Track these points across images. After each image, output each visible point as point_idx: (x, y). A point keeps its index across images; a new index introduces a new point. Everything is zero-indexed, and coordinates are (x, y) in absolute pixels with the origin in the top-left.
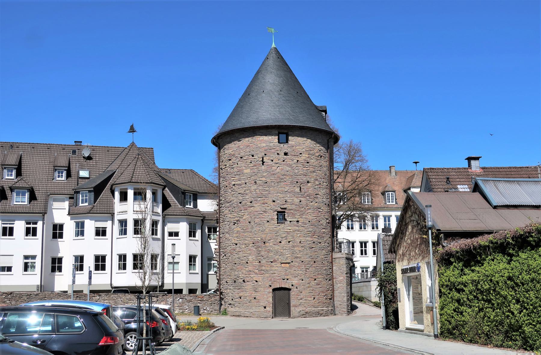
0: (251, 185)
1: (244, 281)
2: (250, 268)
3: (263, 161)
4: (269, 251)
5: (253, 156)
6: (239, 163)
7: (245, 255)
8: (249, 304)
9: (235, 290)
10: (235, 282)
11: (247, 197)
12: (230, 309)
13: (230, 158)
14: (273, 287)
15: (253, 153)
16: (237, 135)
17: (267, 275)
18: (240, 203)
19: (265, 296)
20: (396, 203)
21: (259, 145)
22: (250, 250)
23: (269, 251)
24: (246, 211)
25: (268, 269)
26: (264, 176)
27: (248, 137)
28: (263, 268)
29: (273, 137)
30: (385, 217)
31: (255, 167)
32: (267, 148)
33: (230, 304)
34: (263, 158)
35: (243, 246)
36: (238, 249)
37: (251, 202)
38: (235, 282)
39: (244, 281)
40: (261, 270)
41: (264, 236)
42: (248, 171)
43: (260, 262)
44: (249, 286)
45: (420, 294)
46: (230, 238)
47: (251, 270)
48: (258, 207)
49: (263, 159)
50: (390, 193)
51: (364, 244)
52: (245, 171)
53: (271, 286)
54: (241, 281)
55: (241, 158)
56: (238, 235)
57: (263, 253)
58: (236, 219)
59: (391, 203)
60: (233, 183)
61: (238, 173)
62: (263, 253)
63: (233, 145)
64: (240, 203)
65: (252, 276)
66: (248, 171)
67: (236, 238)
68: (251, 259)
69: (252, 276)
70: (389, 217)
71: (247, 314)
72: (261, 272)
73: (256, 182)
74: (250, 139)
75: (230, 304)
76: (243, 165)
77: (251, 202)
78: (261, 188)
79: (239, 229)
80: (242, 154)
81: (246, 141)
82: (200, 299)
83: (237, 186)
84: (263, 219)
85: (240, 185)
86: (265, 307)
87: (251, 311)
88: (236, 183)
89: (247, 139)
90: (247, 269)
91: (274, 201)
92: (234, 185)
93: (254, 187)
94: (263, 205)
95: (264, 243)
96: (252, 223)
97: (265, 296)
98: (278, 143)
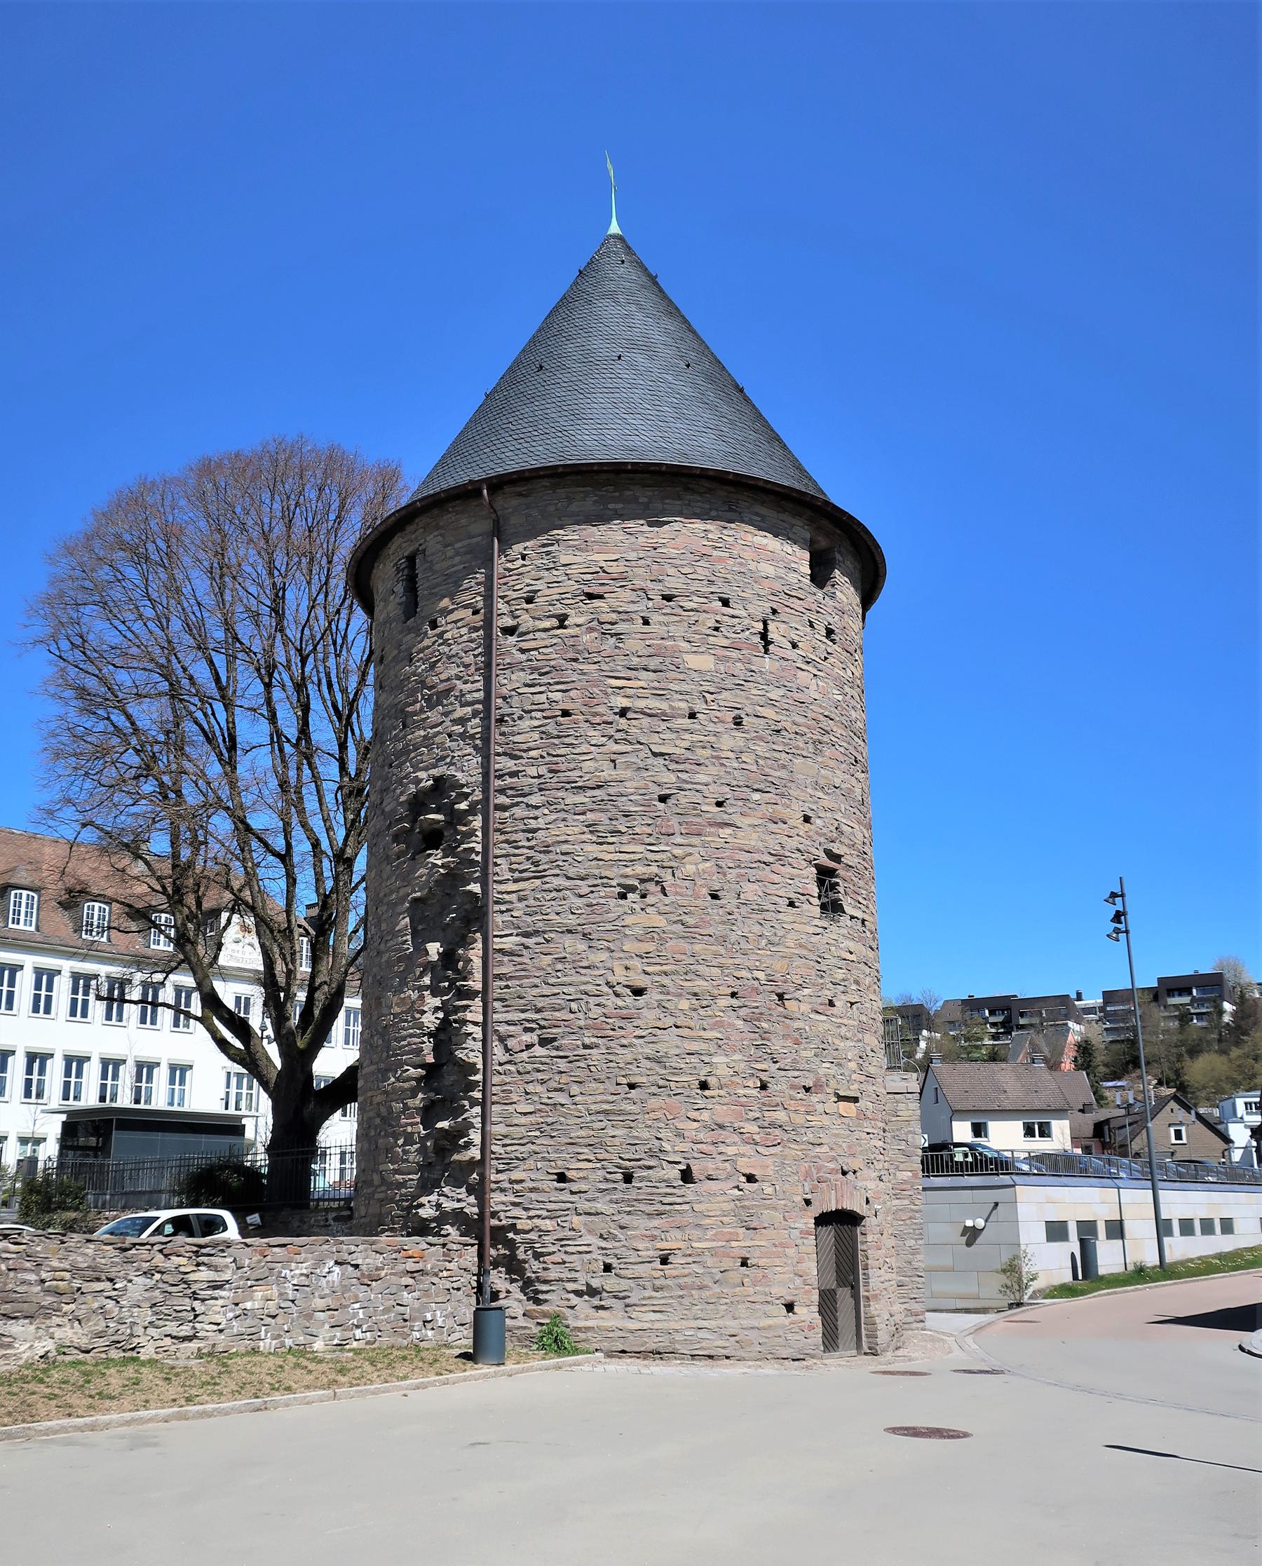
0: (720, 728)
1: (687, 1176)
2: (723, 1113)
3: (764, 635)
4: (799, 1039)
5: (726, 603)
6: (654, 618)
7: (694, 1047)
8: (717, 1289)
9: (625, 1220)
10: (628, 1178)
11: (702, 778)
12: (583, 1315)
13: (596, 590)
14: (816, 1210)
15: (728, 592)
16: (643, 495)
17: (794, 1151)
18: (663, 799)
19: (791, 1252)
20: (38, 929)
21: (752, 566)
22: (718, 1025)
23: (799, 1039)
24: (695, 840)
25: (799, 1119)
26: (772, 703)
27: (704, 516)
28: (781, 1116)
29: (796, 548)
30: (39, 972)
31: (735, 654)
32: (777, 586)
33: (592, 1292)
34: (765, 623)
35: (684, 1004)
36: (649, 1016)
37: (719, 804)
38: (628, 1178)
39: (687, 1176)
40: (773, 1125)
41: (779, 965)
42: (704, 662)
43: (764, 1087)
44: (714, 1199)
45: (1220, 1256)
46: (596, 957)
47: (725, 1120)
48: (750, 834)
49: (765, 628)
50: (25, 893)
51: (36, 1060)
52: (693, 661)
53: (808, 1202)
54: (674, 1173)
55: (668, 598)
56: (650, 947)
57: (776, 1045)
58: (640, 869)
59: (21, 926)
60: (622, 702)
61: (653, 663)
62: (776, 1045)
63: (620, 536)
64: (663, 799)
65: (731, 1150)
66: (704, 662)
67: (636, 963)
68: (723, 1071)
69: (731, 1150)
70: (53, 974)
71: (714, 1343)
72: (773, 1133)
73: (738, 722)
74: (711, 526)
75: (592, 1292)
76: (677, 630)
77: (719, 804)
78: (761, 748)
79: (660, 922)
80: (674, 583)
81: (687, 535)
82: (411, 1266)
83: (646, 721)
84: (772, 889)
85: (664, 717)
86: (790, 1307)
87: (732, 1325)
88: (641, 704)
89: (698, 525)
90: (705, 1116)
91: (807, 819)
92: (623, 712)
93: (730, 740)
94: (772, 827)
95: (781, 996)
96: (728, 900)
97: (791, 1252)
98: (807, 581)
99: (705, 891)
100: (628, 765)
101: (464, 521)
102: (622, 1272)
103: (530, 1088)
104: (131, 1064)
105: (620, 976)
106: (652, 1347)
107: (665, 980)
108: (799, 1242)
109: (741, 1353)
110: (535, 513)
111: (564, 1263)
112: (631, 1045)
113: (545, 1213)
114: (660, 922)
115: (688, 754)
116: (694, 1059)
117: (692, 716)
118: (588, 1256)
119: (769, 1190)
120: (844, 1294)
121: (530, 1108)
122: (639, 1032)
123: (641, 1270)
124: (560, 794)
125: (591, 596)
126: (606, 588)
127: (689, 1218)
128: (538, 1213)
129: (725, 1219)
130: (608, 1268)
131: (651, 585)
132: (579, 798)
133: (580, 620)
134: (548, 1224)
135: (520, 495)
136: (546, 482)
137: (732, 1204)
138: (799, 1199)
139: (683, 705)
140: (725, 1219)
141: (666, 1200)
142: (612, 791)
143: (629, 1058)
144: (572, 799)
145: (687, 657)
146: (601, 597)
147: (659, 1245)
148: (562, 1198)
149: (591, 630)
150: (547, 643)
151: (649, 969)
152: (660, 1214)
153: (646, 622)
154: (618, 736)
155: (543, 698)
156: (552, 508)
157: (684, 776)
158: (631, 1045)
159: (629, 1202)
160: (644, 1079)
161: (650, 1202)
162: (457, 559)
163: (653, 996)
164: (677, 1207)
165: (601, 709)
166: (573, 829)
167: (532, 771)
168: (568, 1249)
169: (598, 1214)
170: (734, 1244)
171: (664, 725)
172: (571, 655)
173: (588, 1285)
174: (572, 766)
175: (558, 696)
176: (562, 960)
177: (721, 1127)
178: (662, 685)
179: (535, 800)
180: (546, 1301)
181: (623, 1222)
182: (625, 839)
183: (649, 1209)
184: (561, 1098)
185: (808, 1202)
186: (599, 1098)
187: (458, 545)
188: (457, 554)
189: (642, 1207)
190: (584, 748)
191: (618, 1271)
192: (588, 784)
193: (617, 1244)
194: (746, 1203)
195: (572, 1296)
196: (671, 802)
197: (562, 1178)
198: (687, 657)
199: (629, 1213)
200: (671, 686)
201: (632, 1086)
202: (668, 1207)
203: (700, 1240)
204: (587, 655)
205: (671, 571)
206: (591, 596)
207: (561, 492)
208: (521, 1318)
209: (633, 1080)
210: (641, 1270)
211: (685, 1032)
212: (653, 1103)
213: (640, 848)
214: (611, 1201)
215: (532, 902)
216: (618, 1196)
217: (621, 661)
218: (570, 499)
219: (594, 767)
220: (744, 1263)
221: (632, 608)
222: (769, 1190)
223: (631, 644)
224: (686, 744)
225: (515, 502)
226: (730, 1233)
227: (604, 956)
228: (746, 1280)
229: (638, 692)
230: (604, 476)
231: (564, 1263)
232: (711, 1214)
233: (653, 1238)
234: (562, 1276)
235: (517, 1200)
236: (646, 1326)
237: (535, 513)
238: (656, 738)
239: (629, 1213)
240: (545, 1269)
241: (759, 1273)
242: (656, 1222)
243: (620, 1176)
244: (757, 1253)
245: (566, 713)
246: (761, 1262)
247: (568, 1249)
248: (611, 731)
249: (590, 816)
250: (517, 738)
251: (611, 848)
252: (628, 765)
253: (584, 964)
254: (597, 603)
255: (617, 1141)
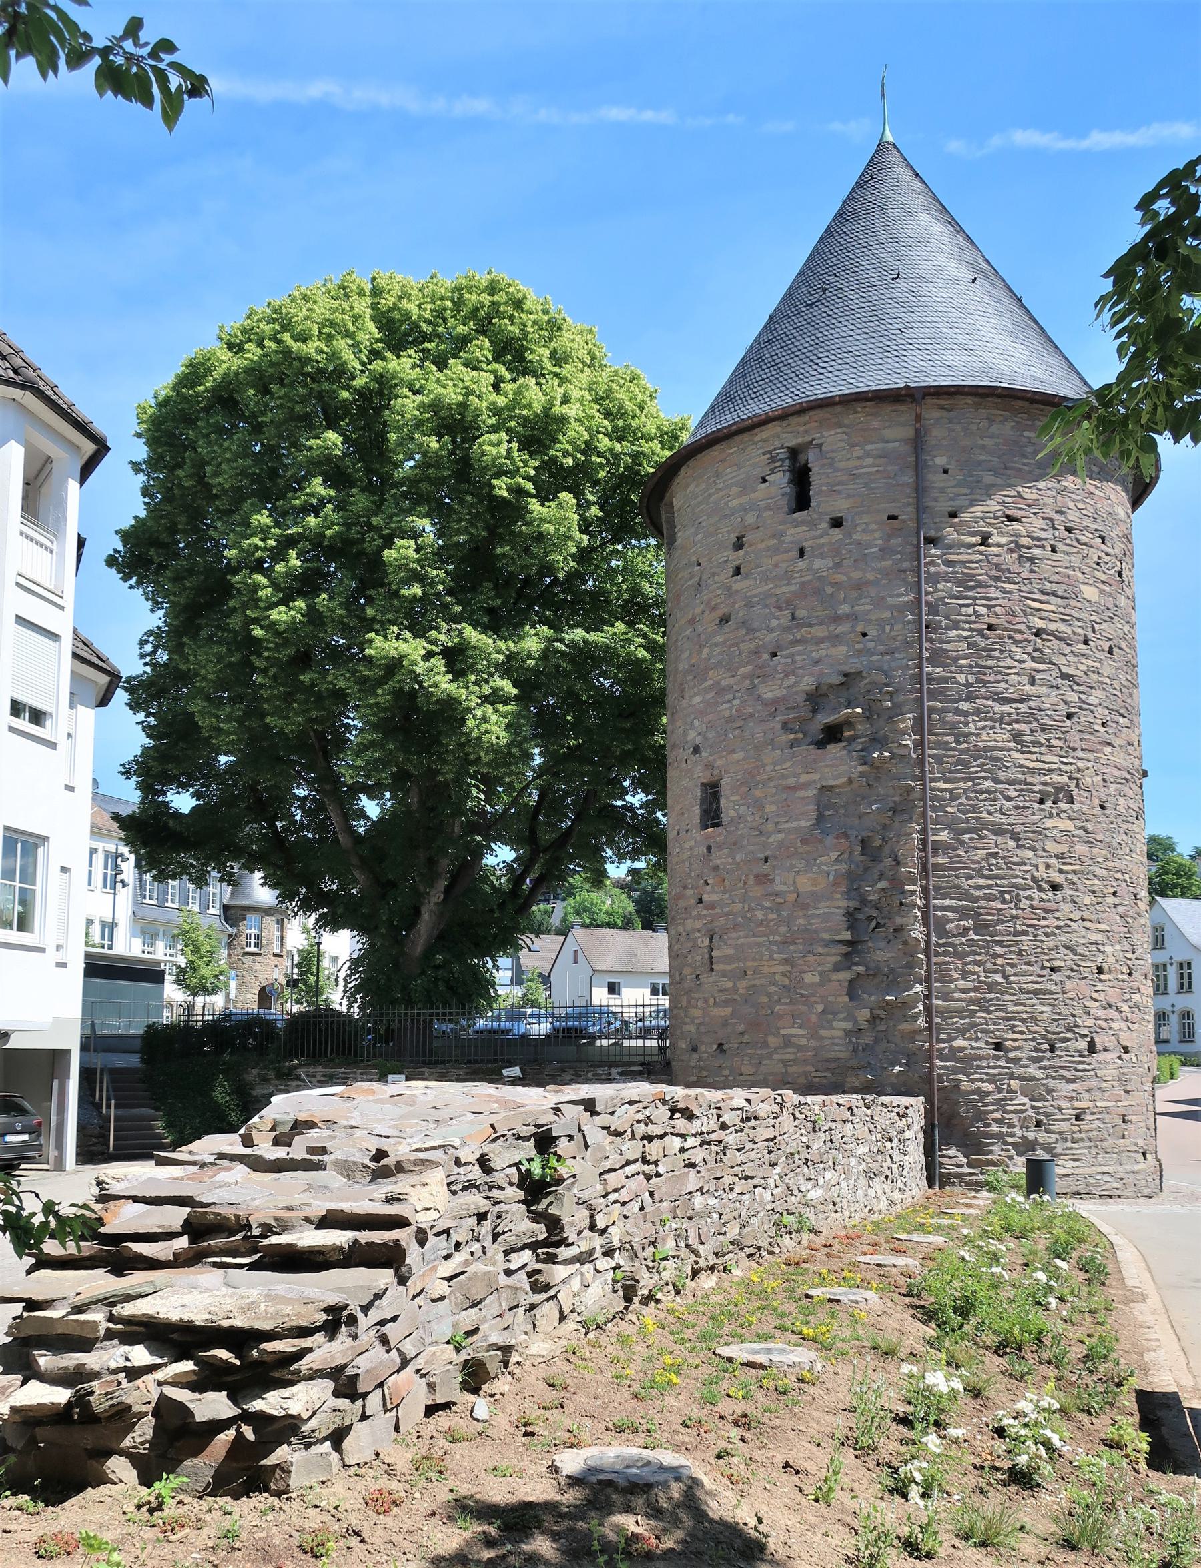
1: (1092, 1048)
6: (1060, 547)
18: (1069, 716)
39: (1092, 1048)
47: (1112, 1001)
54: (1083, 1045)
55: (1068, 529)
60: (1038, 623)
88: (1052, 626)
92: (1037, 634)
99: (1097, 802)
100: (1045, 682)
101: (875, 424)
103: (970, 968)
104: (97, 922)
105: (1041, 873)
106: (1074, 1189)
107: (1075, 878)
109: (1125, 1193)
110: (958, 428)
112: (1053, 934)
114: (1069, 826)
115: (1085, 678)
116: (1093, 948)
117: (1086, 642)
121: (971, 985)
122: (1058, 923)
123: (1064, 1126)
124: (989, 703)
125: (1010, 518)
126: (1021, 513)
130: (1038, 1124)
131: (1056, 516)
132: (1006, 708)
133: (1003, 540)
135: (942, 408)
136: (969, 400)
139: (1080, 631)
141: (1080, 1067)
142: (1033, 704)
143: (1052, 944)
144: (998, 708)
145: (1083, 587)
146: (1017, 520)
149: (1011, 551)
150: (972, 557)
151: (1064, 868)
153: (1053, 550)
154: (1035, 654)
155: (970, 610)
156: (974, 427)
157: (1083, 697)
158: (1053, 934)
160: (1062, 964)
161: (1068, 1069)
162: (869, 461)
163: (1067, 892)
165: (1022, 627)
166: (999, 737)
167: (961, 678)
171: (1069, 649)
172: (994, 573)
174: (999, 677)
175: (983, 610)
176: (995, 855)
177: (1110, 1006)
178: (1067, 611)
179: (965, 706)
182: (1044, 749)
184: (998, 978)
186: (1030, 979)
187: (869, 447)
188: (868, 455)
190: (1009, 662)
192: (1015, 696)
196: (1075, 719)
197: (998, 1046)
198: (1083, 587)
200: (1073, 612)
201: (1052, 970)
204: (1001, 574)
205: (1071, 505)
206: (1010, 518)
207: (983, 412)
208: (408, 1189)
209: (1056, 963)
210: (1064, 1126)
211: (1088, 924)
212: (1069, 984)
213: (1056, 759)
215: (963, 800)
216: (1045, 1063)
217: (1036, 585)
218: (991, 420)
219: (1017, 683)
221: (1043, 535)
223: (1045, 568)
224: (1084, 668)
225: (936, 414)
227: (1030, 854)
229: (1047, 614)
230: (1020, 403)
236: (1070, 1172)
237: (958, 428)
238: (1062, 660)
242: (1073, 1086)
243: (1046, 1047)
245: (991, 627)
248: (1029, 649)
249: (1015, 726)
250: (945, 646)
251: (1033, 757)
252: (1045, 682)
253: (1015, 859)
254: (1015, 525)
255: (1045, 1016)
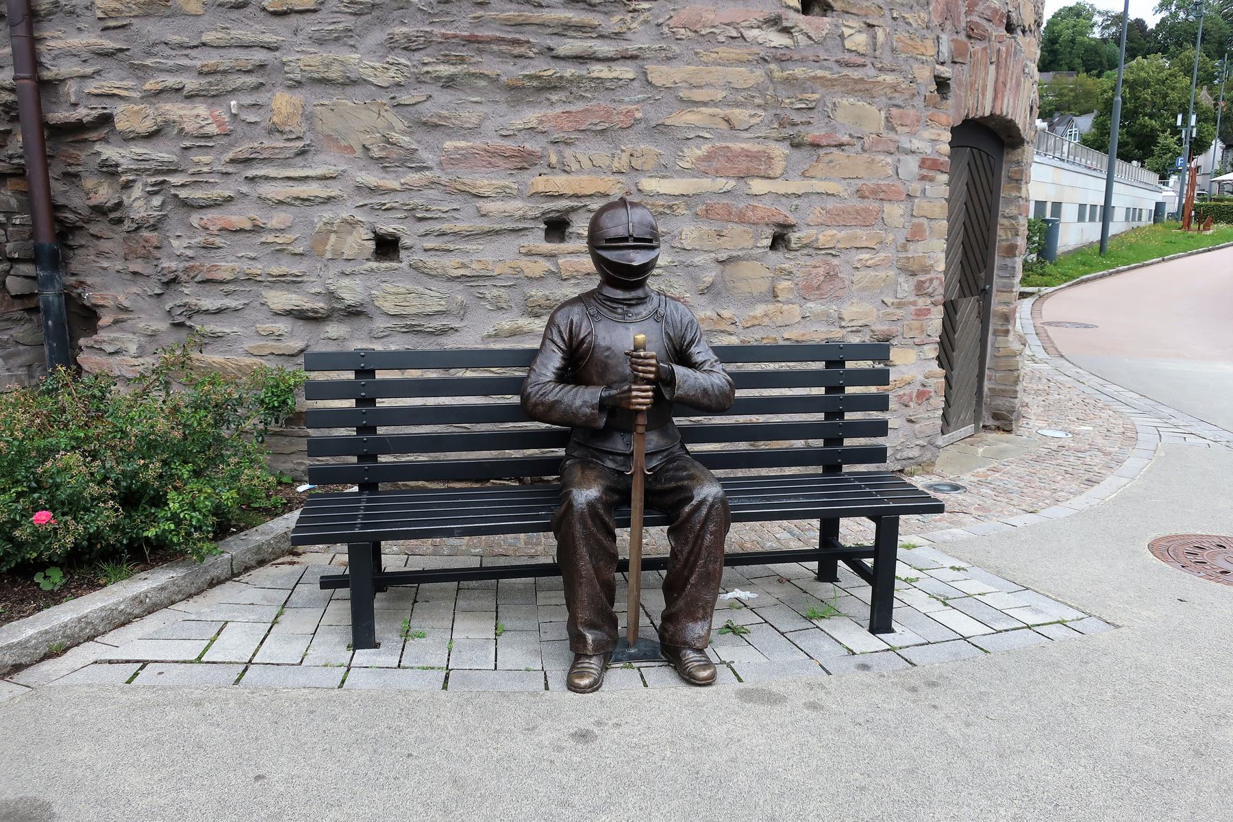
9: (440, 103)
19: (895, 212)
102: (431, 261)
108: (916, 187)
111: (257, 229)
113: (191, 83)
118: (326, 214)
119: (859, 40)
120: (969, 308)
127: (632, 103)
128: (171, 81)
129: (741, 115)
130: (387, 247)
134: (196, 116)
137: (758, 74)
138: (924, 75)
140: (741, 115)
141: (569, 46)
147: (541, 183)
148: (247, 35)
152: (548, 86)
159: (448, 48)
161: (514, 49)
164: (599, 70)
168: (267, 190)
169: (354, 83)
170: (758, 186)
173: (331, 295)
180: (216, 337)
181: (429, 111)
183: (511, 71)
185: (942, 85)
189: (490, 66)
191: (417, 257)
193: (413, 178)
194: (799, 71)
195: (282, 326)
199: (449, 83)
202: (569, 71)
203: (664, 171)
214: (392, 45)
220: (779, 241)
222: (859, 40)
226: (748, 155)
228: (783, 285)
231: (257, 229)
232: (697, 95)
233: (525, 162)
234: (257, 268)
235: (109, 44)
239: (449, 83)
240: (208, 247)
241: (815, 267)
242: (531, 116)
244: (814, 213)
246: (826, 237)
247: (267, 190)
